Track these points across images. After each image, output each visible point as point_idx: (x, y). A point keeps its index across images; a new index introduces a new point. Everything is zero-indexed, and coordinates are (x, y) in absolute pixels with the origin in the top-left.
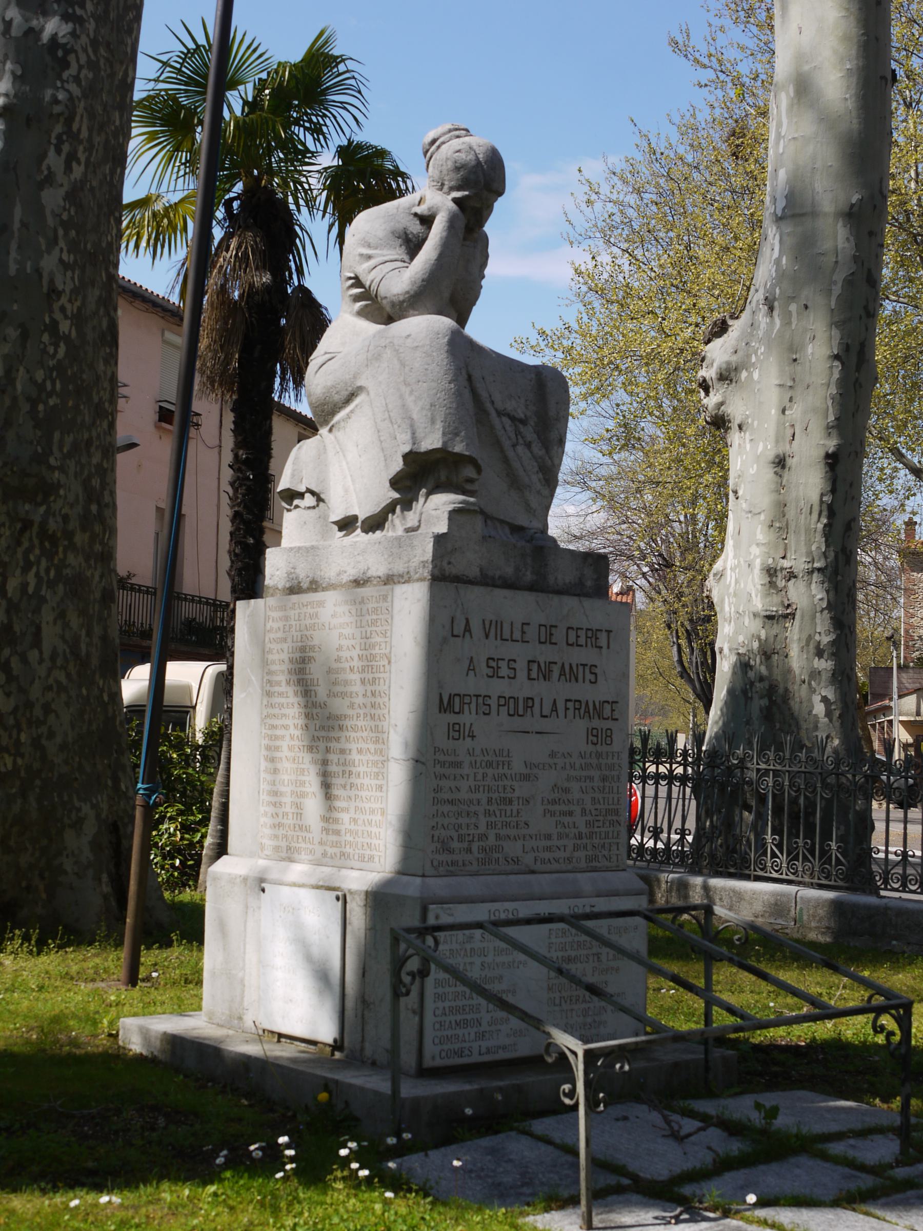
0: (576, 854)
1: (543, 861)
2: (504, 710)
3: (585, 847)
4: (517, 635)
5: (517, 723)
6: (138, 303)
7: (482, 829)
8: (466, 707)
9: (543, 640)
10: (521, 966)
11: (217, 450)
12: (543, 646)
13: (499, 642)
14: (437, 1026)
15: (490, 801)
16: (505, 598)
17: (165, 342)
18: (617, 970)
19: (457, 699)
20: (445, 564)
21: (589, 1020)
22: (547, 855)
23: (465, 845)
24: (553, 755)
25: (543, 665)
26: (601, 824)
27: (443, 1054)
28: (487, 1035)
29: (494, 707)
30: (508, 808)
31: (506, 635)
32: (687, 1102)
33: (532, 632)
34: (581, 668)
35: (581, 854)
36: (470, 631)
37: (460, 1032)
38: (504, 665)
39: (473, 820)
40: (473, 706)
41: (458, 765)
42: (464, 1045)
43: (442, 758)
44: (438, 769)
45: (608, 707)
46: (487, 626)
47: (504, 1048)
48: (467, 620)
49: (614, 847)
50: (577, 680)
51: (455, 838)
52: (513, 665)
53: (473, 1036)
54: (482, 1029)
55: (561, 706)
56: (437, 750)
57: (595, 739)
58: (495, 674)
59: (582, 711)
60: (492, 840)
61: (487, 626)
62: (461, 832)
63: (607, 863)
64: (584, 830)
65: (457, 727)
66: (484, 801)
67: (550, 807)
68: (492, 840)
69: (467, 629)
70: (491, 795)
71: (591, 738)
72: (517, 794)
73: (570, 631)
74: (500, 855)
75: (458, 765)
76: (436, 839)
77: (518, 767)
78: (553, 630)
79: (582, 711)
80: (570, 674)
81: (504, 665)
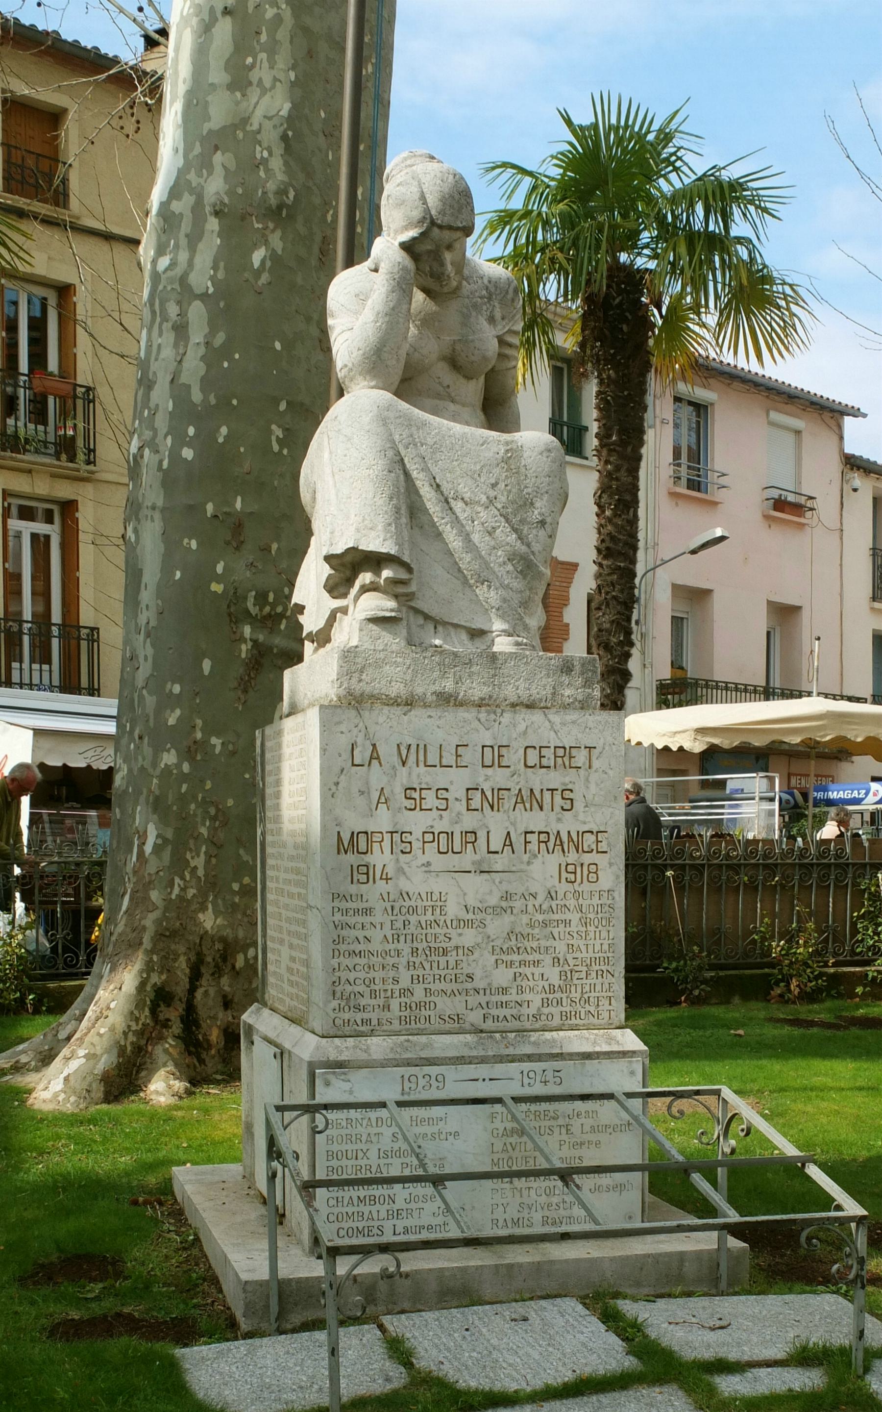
0: (546, 1011)
1: (496, 1019)
2: (431, 848)
3: (560, 1002)
4: (449, 759)
5: (452, 861)
6: (736, 384)
7: (405, 982)
8: (376, 846)
9: (488, 762)
10: (451, 1138)
11: (838, 533)
12: (489, 771)
13: (422, 768)
14: (332, 1202)
15: (414, 951)
16: (430, 717)
17: (772, 424)
18: (598, 1144)
19: (362, 838)
20: (354, 680)
21: (555, 1200)
22: (501, 1012)
23: (381, 1002)
24: (507, 896)
25: (489, 794)
26: (583, 975)
27: (342, 1233)
28: (404, 1214)
29: (417, 845)
30: (443, 960)
31: (433, 759)
32: (158, 1346)
33: (470, 756)
34: (547, 795)
35: (555, 1010)
36: (378, 758)
37: (366, 1209)
38: (429, 796)
39: (392, 974)
40: (386, 844)
41: (368, 911)
42: (371, 1223)
43: (344, 905)
44: (338, 917)
45: (590, 839)
46: (404, 752)
47: (430, 1228)
48: (374, 745)
49: (604, 1002)
50: (541, 809)
51: (367, 994)
52: (567, 794)
53: (383, 1214)
54: (396, 1207)
55: (518, 840)
56: (336, 896)
57: (572, 877)
58: (418, 806)
59: (551, 845)
60: (419, 994)
61: (404, 752)
62: (373, 986)
63: (595, 1021)
64: (556, 981)
65: (571, 868)
66: (407, 951)
67: (505, 957)
68: (419, 994)
69: (375, 756)
70: (415, 944)
71: (564, 875)
72: (453, 943)
73: (529, 750)
74: (432, 1013)
75: (368, 911)
76: (338, 995)
77: (453, 910)
78: (504, 751)
79: (551, 845)
80: (531, 799)
81: (429, 796)
